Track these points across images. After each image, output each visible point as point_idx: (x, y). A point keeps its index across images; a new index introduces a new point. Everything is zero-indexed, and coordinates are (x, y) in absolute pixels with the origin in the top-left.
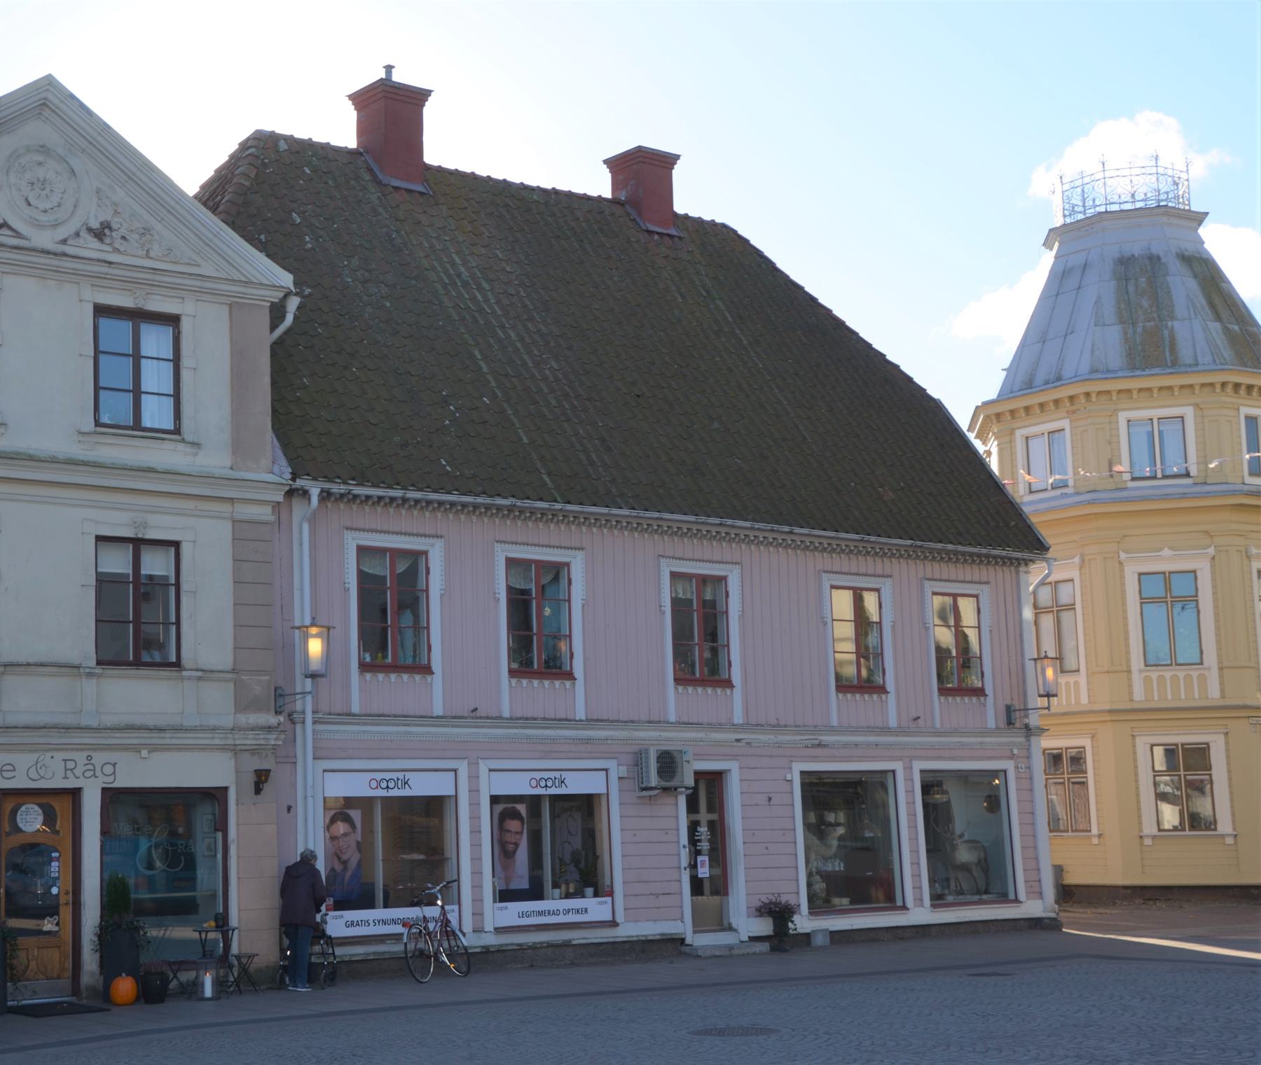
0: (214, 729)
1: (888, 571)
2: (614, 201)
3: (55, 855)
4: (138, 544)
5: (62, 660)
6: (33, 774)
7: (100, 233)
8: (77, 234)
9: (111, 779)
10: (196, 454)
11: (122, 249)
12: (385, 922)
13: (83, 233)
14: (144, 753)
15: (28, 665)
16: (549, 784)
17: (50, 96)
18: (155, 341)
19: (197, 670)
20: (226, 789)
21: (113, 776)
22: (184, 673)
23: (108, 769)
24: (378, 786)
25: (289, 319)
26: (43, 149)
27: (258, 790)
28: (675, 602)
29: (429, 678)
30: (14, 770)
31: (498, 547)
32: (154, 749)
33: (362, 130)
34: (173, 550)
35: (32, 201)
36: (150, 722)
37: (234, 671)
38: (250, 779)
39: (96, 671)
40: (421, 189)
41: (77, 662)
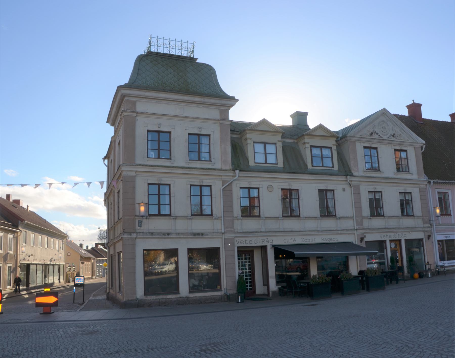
0: (421, 227)
1: (450, 188)
2: (409, 117)
3: (397, 252)
4: (375, 192)
5: (314, 216)
6: (255, 242)
7: (393, 136)
8: (390, 136)
9: (405, 237)
10: (412, 176)
11: (397, 138)
12: (448, 263)
13: (391, 136)
14: (410, 232)
15: (391, 217)
16: (447, 237)
17: (385, 112)
18: (374, 151)
19: (417, 216)
20: (423, 239)
21: (256, 243)
22: (261, 218)
23: (405, 236)
24: (445, 238)
25: (424, 149)
26: (383, 121)
27: (428, 239)
28: (439, 198)
29: (451, 216)
30: (252, 242)
31: (436, 190)
32: (412, 231)
33: (409, 112)
34: (333, 191)
35: (383, 131)
36: (410, 226)
37: (422, 216)
38: (427, 237)
39: (320, 218)
40: (423, 123)
41: (398, 216)
